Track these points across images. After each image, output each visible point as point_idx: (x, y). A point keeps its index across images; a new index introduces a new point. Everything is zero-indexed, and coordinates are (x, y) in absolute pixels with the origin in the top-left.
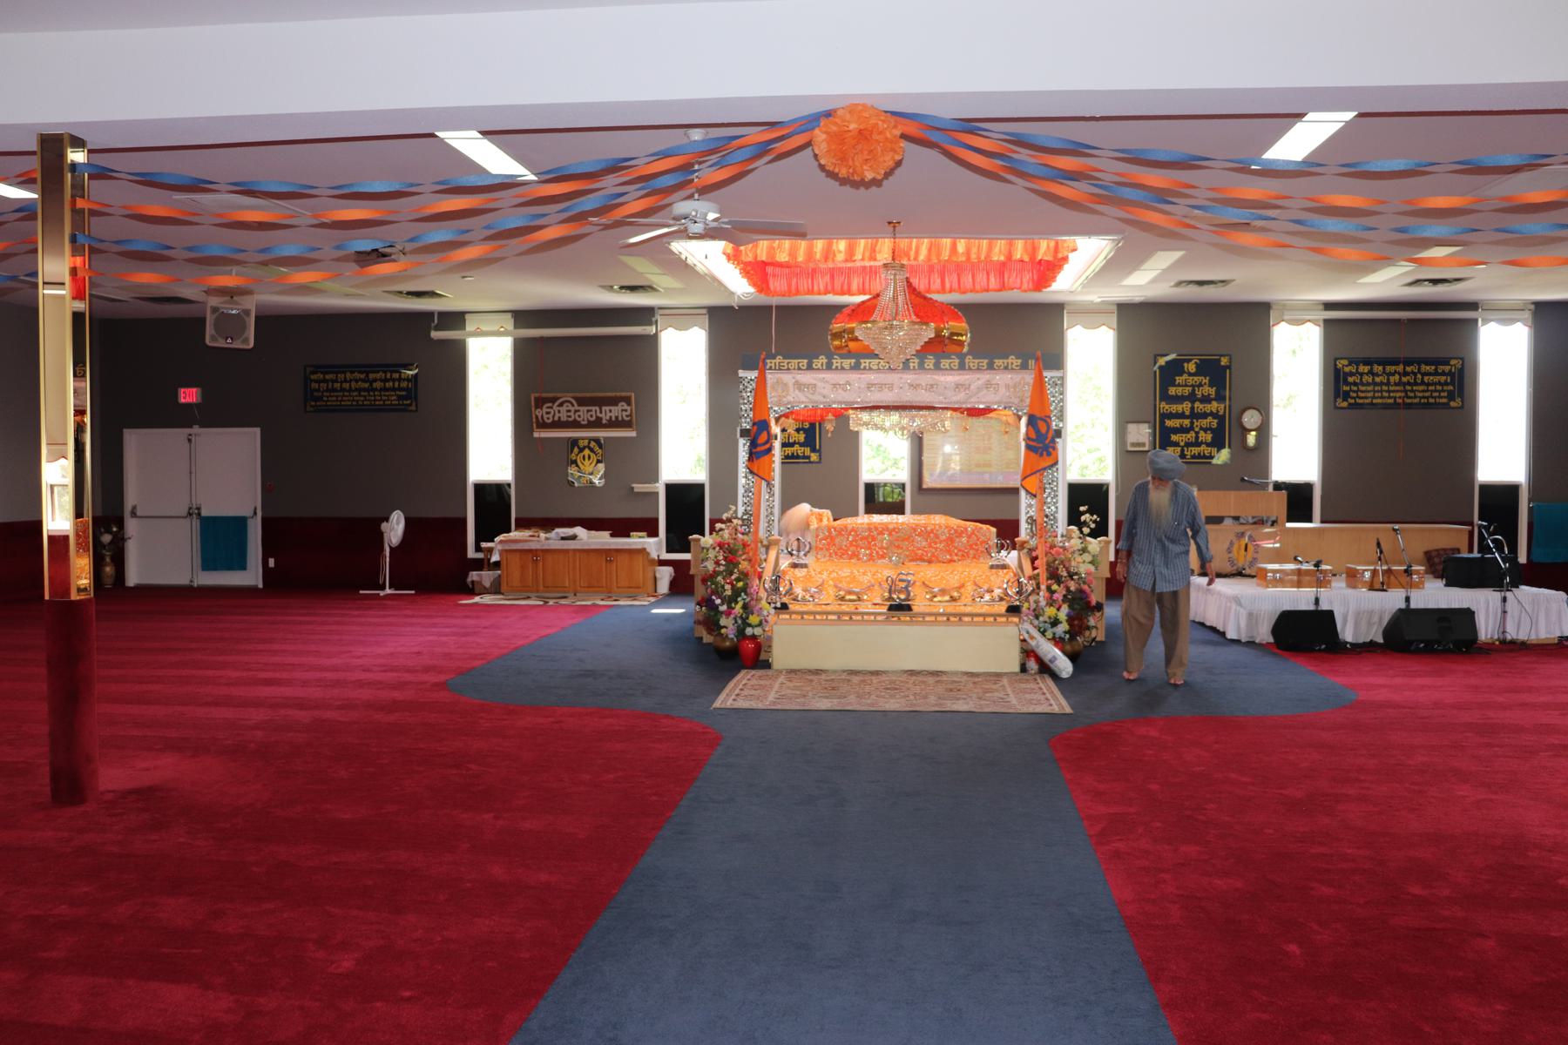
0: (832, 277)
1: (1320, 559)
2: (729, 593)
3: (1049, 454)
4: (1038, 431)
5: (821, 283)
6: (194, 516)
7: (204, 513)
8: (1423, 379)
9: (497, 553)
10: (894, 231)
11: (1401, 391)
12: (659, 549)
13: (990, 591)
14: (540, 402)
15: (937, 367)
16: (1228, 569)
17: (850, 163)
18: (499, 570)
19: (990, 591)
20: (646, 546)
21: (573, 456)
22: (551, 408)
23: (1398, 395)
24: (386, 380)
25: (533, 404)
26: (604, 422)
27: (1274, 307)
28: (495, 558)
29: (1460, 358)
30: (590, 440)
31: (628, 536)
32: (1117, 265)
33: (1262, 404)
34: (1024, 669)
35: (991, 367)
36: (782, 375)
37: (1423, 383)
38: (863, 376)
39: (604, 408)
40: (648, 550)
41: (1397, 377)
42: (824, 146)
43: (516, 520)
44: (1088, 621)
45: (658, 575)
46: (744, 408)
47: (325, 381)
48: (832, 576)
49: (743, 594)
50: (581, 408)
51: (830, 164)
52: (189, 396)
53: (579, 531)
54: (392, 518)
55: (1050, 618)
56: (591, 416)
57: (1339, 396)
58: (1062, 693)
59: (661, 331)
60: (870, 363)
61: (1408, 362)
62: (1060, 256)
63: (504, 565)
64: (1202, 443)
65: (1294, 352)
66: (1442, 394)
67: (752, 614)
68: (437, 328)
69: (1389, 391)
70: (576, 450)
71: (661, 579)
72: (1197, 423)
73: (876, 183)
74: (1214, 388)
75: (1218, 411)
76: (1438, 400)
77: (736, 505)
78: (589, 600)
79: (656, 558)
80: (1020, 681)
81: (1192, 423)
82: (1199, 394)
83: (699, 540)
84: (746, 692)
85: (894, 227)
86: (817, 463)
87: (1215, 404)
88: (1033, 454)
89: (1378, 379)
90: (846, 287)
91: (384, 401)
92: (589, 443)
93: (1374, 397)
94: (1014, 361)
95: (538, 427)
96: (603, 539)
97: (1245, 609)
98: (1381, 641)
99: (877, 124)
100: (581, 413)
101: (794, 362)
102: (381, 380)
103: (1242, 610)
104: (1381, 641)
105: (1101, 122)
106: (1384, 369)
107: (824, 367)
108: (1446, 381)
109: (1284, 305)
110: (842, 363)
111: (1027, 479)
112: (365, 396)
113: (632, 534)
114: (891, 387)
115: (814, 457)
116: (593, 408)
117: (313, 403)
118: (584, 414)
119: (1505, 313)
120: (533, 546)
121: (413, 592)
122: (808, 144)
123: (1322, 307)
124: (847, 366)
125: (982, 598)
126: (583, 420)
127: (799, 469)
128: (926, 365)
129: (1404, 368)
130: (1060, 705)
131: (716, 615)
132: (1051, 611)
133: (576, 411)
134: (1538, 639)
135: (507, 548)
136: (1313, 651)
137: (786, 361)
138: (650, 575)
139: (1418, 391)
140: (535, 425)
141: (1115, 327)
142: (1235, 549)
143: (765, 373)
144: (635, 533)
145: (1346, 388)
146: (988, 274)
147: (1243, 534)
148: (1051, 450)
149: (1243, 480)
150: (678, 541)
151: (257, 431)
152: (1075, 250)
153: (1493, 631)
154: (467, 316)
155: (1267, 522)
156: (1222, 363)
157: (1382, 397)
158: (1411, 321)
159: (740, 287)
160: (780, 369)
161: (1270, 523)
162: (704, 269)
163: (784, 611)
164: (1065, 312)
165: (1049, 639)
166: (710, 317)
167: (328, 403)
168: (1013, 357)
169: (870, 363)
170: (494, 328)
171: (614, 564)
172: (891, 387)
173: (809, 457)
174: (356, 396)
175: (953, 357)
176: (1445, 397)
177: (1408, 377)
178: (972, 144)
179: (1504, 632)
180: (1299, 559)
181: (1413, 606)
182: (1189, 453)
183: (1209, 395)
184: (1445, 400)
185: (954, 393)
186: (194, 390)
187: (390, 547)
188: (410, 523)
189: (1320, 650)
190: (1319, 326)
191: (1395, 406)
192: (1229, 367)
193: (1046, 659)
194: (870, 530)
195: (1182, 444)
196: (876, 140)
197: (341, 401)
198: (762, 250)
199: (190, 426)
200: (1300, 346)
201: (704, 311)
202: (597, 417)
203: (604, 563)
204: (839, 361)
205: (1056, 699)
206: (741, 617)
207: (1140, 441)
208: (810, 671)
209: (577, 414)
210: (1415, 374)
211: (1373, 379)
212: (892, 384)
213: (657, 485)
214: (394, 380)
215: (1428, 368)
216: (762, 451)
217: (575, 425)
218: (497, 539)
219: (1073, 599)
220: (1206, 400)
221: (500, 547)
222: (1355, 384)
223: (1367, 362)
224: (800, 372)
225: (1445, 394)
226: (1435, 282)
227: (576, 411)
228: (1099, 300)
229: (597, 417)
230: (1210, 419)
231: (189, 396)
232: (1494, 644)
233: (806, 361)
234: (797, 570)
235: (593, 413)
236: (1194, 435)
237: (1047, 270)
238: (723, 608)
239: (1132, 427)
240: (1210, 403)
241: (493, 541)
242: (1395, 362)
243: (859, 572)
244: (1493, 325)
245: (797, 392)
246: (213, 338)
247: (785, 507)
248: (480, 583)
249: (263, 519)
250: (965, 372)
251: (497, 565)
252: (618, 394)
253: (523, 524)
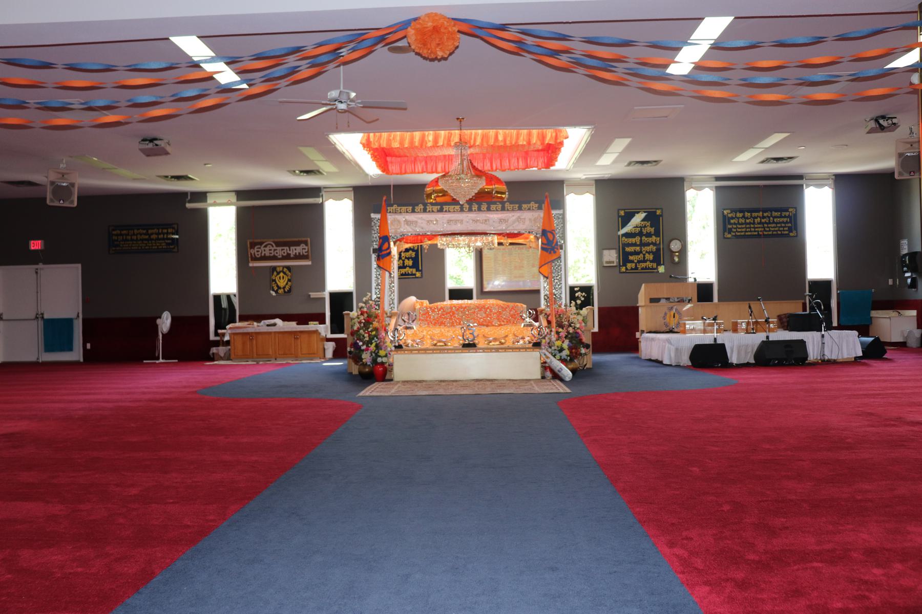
0: (426, 163)
1: (715, 315)
2: (367, 339)
3: (555, 252)
4: (548, 239)
5: (419, 167)
6: (40, 319)
7: (46, 317)
8: (773, 220)
9: (228, 335)
10: (460, 123)
11: (762, 228)
12: (326, 331)
13: (523, 338)
14: (253, 245)
15: (489, 209)
16: (664, 329)
17: (429, 46)
18: (230, 346)
19: (523, 338)
20: (318, 329)
21: (273, 277)
22: (260, 248)
23: (760, 229)
24: (158, 234)
25: (249, 246)
26: (292, 256)
27: (687, 180)
28: (227, 338)
29: (794, 208)
30: (284, 267)
31: (308, 324)
32: (593, 149)
33: (682, 237)
34: (543, 377)
35: (520, 209)
36: (397, 216)
37: (774, 222)
38: (445, 216)
39: (291, 248)
40: (320, 331)
41: (759, 219)
42: (413, 38)
43: (240, 316)
44: (581, 350)
45: (326, 347)
46: (375, 236)
47: (121, 235)
48: (429, 333)
49: (375, 338)
50: (278, 248)
51: (417, 48)
52: (36, 245)
53: (278, 321)
54: (163, 316)
55: (558, 347)
56: (284, 253)
58: (567, 387)
59: (325, 201)
60: (449, 208)
61: (765, 211)
62: (559, 141)
63: (232, 343)
64: (647, 260)
65: (704, 227)
66: (785, 229)
67: (381, 350)
68: (190, 202)
69: (754, 228)
70: (275, 273)
71: (328, 349)
72: (645, 249)
73: (446, 59)
74: (653, 228)
75: (656, 242)
76: (783, 232)
77: (371, 292)
78: (284, 361)
79: (325, 336)
80: (541, 382)
81: (641, 249)
82: (644, 232)
83: (349, 314)
84: (377, 390)
85: (461, 121)
86: (420, 278)
87: (654, 238)
88: (545, 252)
89: (748, 221)
90: (434, 169)
91: (158, 246)
92: (283, 269)
93: (746, 231)
94: (534, 205)
95: (252, 260)
96: (292, 326)
97: (673, 346)
98: (754, 362)
99: (443, 23)
100: (278, 251)
101: (404, 208)
102: (156, 234)
103: (672, 347)
104: (754, 362)
105: (572, 24)
106: (751, 215)
107: (422, 211)
108: (787, 221)
109: (692, 179)
110: (432, 208)
111: (543, 267)
112: (146, 244)
113: (309, 323)
114: (461, 221)
115: (418, 274)
116: (285, 248)
117: (114, 249)
118: (280, 251)
119: (819, 181)
120: (250, 330)
121: (177, 361)
122: (405, 37)
123: (714, 179)
124: (435, 210)
125: (518, 342)
126: (279, 255)
127: (409, 282)
129: (763, 214)
130: (564, 389)
131: (359, 353)
132: (559, 343)
133: (275, 250)
134: (843, 359)
135: (234, 331)
136: (714, 367)
137: (399, 208)
138: (321, 347)
139: (771, 227)
140: (250, 259)
141: (594, 193)
142: (668, 317)
143: (386, 215)
144: (312, 322)
145: (730, 226)
146: (518, 159)
147: (672, 308)
148: (556, 250)
149: (671, 277)
150: (338, 325)
151: (79, 266)
152: (567, 137)
153: (817, 355)
154: (208, 194)
155: (686, 301)
156: (658, 214)
157: (751, 231)
158: (765, 186)
159: (371, 169)
160: (395, 213)
161: (688, 301)
162: (350, 156)
163: (400, 349)
164: (565, 185)
165: (558, 360)
166: (354, 193)
167: (124, 248)
168: (533, 203)
169: (449, 208)
170: (225, 201)
171: (299, 340)
172: (461, 221)
173: (415, 275)
174: (141, 244)
175: (498, 203)
176: (787, 231)
177: (765, 219)
178: (498, 36)
179: (823, 355)
180: (705, 318)
181: (771, 339)
182: (640, 267)
183: (650, 232)
184: (787, 232)
185: (499, 225)
187: (163, 334)
188: (174, 319)
189: (718, 367)
190: (713, 190)
191: (759, 236)
192: (661, 216)
193: (556, 370)
194: (451, 308)
195: (636, 261)
196: (443, 33)
197: (132, 246)
198: (384, 141)
199: (37, 264)
200: (707, 223)
201: (351, 189)
202: (287, 253)
203: (293, 339)
204: (431, 207)
205: (561, 386)
206: (374, 352)
207: (611, 260)
208: (416, 381)
209: (275, 252)
210: (769, 217)
211: (745, 221)
212: (462, 220)
213: (324, 293)
214: (164, 234)
215: (776, 213)
216: (385, 254)
217: (274, 258)
218: (228, 327)
219: (572, 337)
220: (649, 235)
221: (229, 331)
222: (735, 224)
223: (741, 211)
224: (408, 214)
225: (787, 229)
226: (778, 159)
227: (275, 250)
228: (584, 177)
229: (287, 253)
230: (651, 246)
231: (36, 245)
232: (818, 362)
233: (411, 208)
234: (408, 330)
235: (285, 251)
236: (642, 256)
237: (551, 151)
238: (364, 347)
239: (606, 252)
240: (652, 237)
241: (225, 329)
242: (757, 211)
243: (445, 330)
244: (812, 188)
245: (406, 226)
246: (52, 201)
247: (401, 299)
248: (218, 354)
249: (83, 320)
250: (505, 212)
251: (228, 343)
252: (300, 239)
253: (243, 318)
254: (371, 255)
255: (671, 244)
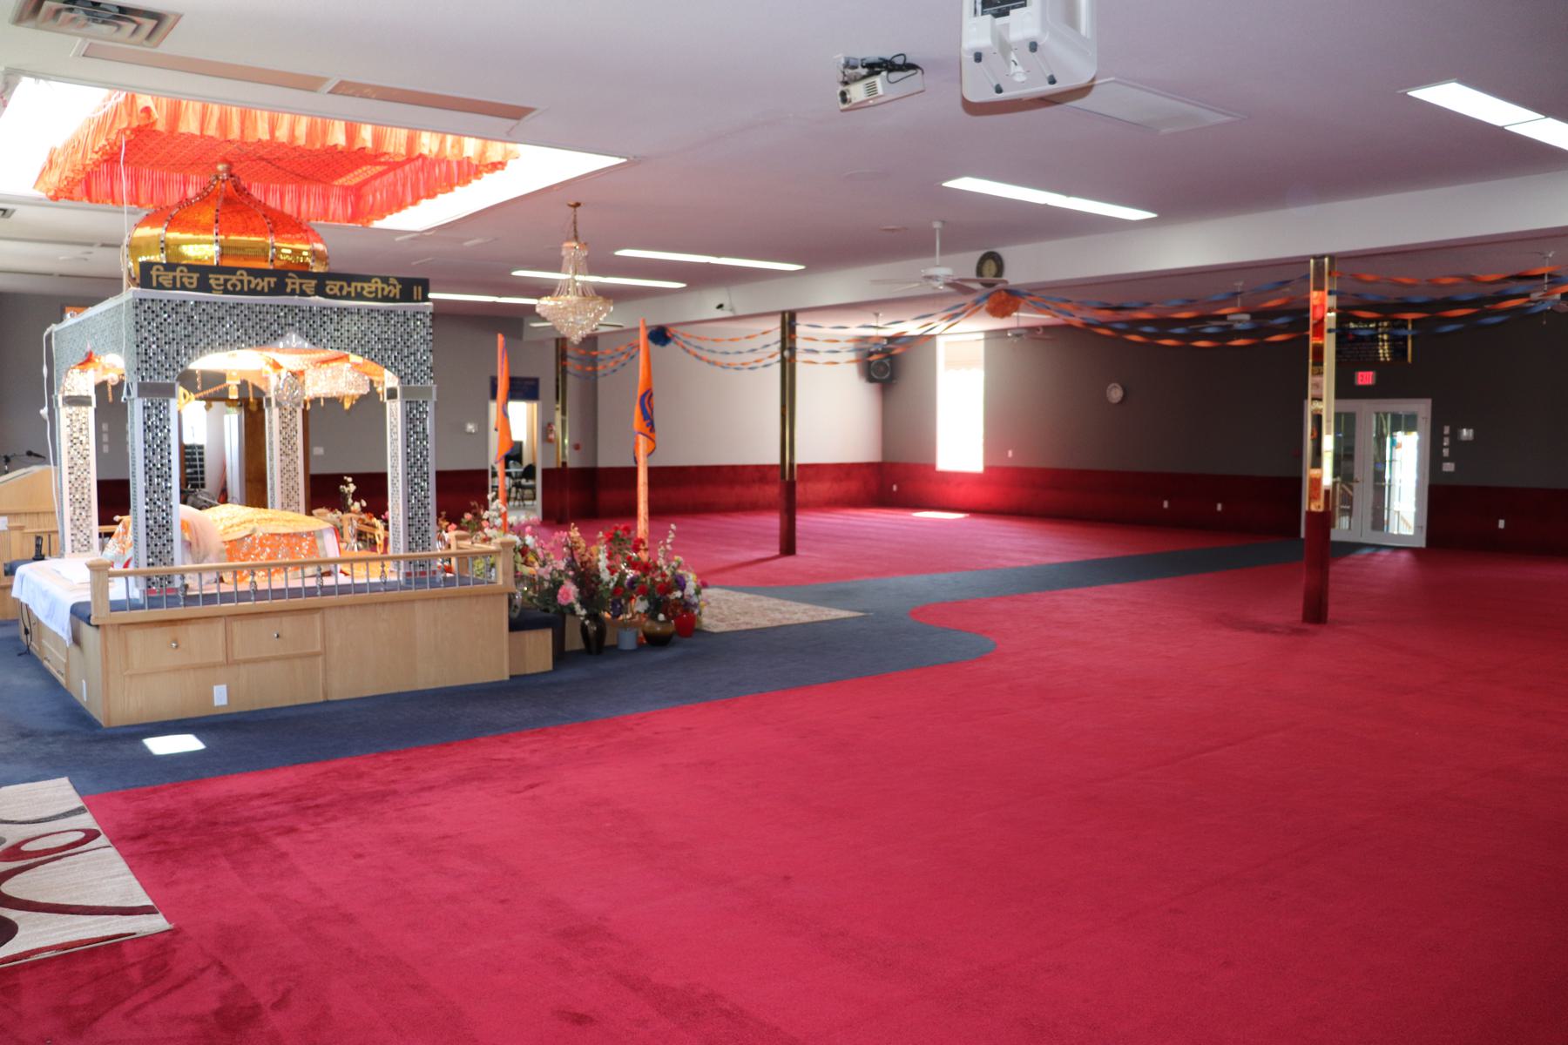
57: (1327, 492)
110: (301, 284)
128: (327, 290)
151: (1429, 401)
186: (1371, 373)
204: (298, 281)
254: (384, 405)
255: (1119, 399)
